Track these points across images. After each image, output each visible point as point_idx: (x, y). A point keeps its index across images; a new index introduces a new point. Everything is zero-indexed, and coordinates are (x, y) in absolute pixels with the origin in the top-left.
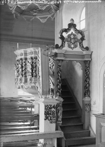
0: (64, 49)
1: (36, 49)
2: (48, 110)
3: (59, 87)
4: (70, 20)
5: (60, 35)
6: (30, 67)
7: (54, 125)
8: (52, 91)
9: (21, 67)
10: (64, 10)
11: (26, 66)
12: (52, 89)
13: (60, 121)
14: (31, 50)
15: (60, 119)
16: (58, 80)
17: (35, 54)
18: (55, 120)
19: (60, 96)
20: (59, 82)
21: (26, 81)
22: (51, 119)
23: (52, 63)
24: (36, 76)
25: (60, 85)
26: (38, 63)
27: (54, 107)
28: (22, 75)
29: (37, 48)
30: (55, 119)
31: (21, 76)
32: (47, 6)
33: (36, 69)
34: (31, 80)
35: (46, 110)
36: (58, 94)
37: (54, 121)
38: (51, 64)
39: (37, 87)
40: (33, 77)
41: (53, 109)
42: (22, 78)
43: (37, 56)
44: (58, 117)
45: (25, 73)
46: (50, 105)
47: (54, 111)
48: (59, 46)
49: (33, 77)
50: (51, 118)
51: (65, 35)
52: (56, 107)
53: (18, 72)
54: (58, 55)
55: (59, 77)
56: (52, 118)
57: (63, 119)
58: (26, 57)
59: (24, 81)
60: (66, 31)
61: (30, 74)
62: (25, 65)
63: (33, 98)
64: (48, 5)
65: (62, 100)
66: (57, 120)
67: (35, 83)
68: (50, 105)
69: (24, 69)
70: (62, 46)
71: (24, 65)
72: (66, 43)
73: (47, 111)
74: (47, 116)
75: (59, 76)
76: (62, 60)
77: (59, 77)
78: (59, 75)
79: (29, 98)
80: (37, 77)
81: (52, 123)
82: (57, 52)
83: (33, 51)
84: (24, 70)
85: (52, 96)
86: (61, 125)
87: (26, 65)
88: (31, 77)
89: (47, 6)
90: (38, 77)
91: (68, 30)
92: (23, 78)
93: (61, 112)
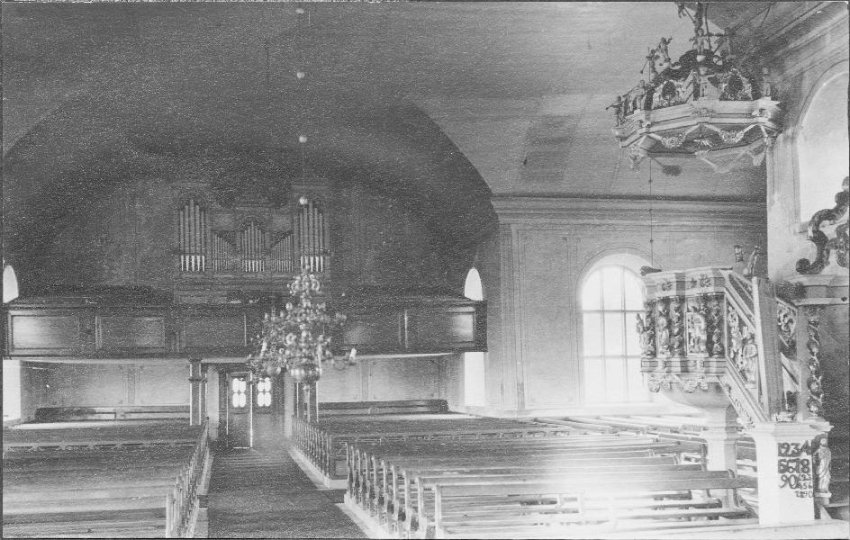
0: (826, 270)
1: (723, 272)
2: (788, 459)
3: (814, 386)
4: (842, 181)
5: (814, 232)
6: (700, 327)
7: (809, 502)
8: (792, 399)
9: (665, 325)
10: (800, 139)
11: (682, 323)
12: (789, 393)
13: (826, 492)
14: (704, 273)
15: (824, 485)
16: (811, 367)
17: (716, 285)
18: (810, 487)
19: (819, 414)
20: (816, 372)
21: (685, 369)
22: (798, 486)
23: (785, 316)
24: (722, 353)
25: (819, 381)
26: (729, 311)
27: (806, 447)
28: (671, 348)
29: (722, 267)
30: (812, 485)
31: (669, 353)
32: (746, 130)
33: (721, 329)
34: (705, 364)
35: (782, 458)
36: (814, 408)
37: (808, 490)
38: (782, 319)
39: (730, 388)
40: (711, 355)
41: (804, 456)
42: (672, 360)
43: (725, 291)
44: (817, 479)
45: (682, 343)
46: (793, 444)
47: (807, 460)
48: (811, 263)
49: (711, 355)
50: (797, 479)
51: (829, 230)
52: (813, 448)
53: (650, 340)
54: (809, 290)
55: (815, 358)
56: (802, 483)
57: (832, 487)
58: (681, 292)
59: (679, 369)
60: (828, 215)
61: (703, 348)
62: (679, 318)
63: (702, 422)
64: (752, 126)
65: (826, 427)
66: (816, 489)
67: (719, 374)
68: (793, 444)
69: (676, 331)
70: (821, 262)
71: (675, 320)
72: (833, 251)
73: (784, 461)
74: (786, 477)
75: (812, 353)
76: (823, 307)
77: (815, 358)
78: (815, 350)
79: (628, 417)
80: (724, 357)
81: (802, 497)
82: (805, 284)
83: (711, 276)
84: (678, 334)
85: (790, 414)
86: (827, 502)
87: (681, 318)
88: (707, 355)
89: (746, 130)
90: (729, 356)
91: (837, 212)
92: (676, 360)
93: (824, 464)
